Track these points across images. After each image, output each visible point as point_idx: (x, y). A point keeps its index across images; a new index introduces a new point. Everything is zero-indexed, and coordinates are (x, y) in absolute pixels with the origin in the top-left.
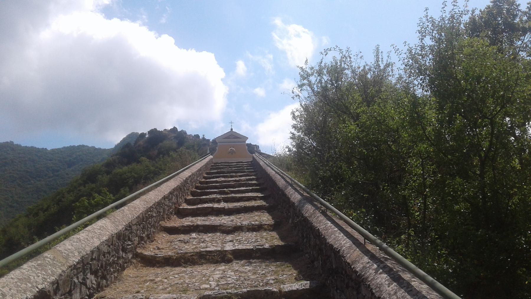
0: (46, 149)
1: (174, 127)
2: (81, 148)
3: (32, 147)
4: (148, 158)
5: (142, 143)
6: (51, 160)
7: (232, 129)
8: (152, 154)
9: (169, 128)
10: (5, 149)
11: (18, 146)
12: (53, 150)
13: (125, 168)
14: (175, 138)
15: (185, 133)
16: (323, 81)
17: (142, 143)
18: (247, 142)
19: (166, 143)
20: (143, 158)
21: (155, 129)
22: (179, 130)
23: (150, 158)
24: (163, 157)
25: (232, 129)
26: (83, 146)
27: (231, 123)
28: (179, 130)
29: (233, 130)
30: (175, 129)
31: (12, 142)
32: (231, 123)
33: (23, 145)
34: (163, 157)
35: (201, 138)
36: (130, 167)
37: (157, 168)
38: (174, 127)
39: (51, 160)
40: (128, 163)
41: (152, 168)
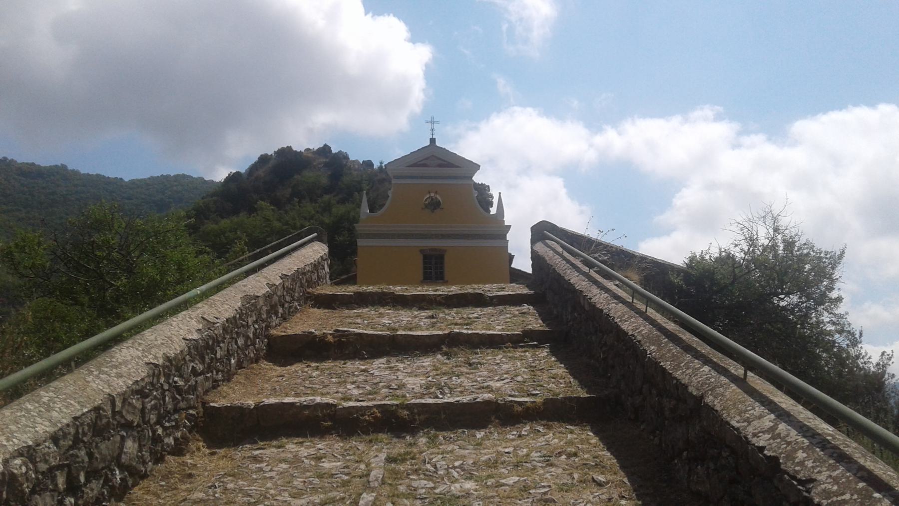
0: (121, 179)
1: (325, 145)
2: (59, 173)
3: (98, 175)
4: (271, 204)
5: (262, 175)
6: (129, 199)
7: (433, 141)
8: (305, 194)
9: (315, 145)
10: (52, 178)
11: (76, 173)
12: (133, 182)
13: (225, 223)
14: (326, 165)
15: (346, 157)
16: (102, 482)
17: (262, 175)
18: (478, 178)
19: (309, 175)
20: (261, 203)
21: (289, 148)
22: (334, 151)
23: (277, 203)
24: (299, 202)
25: (433, 141)
26: (184, 176)
27: (432, 122)
28: (334, 151)
29: (438, 144)
30: (325, 150)
31: (64, 167)
32: (432, 122)
33: (83, 171)
34: (299, 202)
35: (375, 167)
36: (235, 219)
37: (287, 224)
38: (325, 145)
39: (129, 199)
40: (236, 212)
41: (277, 224)
